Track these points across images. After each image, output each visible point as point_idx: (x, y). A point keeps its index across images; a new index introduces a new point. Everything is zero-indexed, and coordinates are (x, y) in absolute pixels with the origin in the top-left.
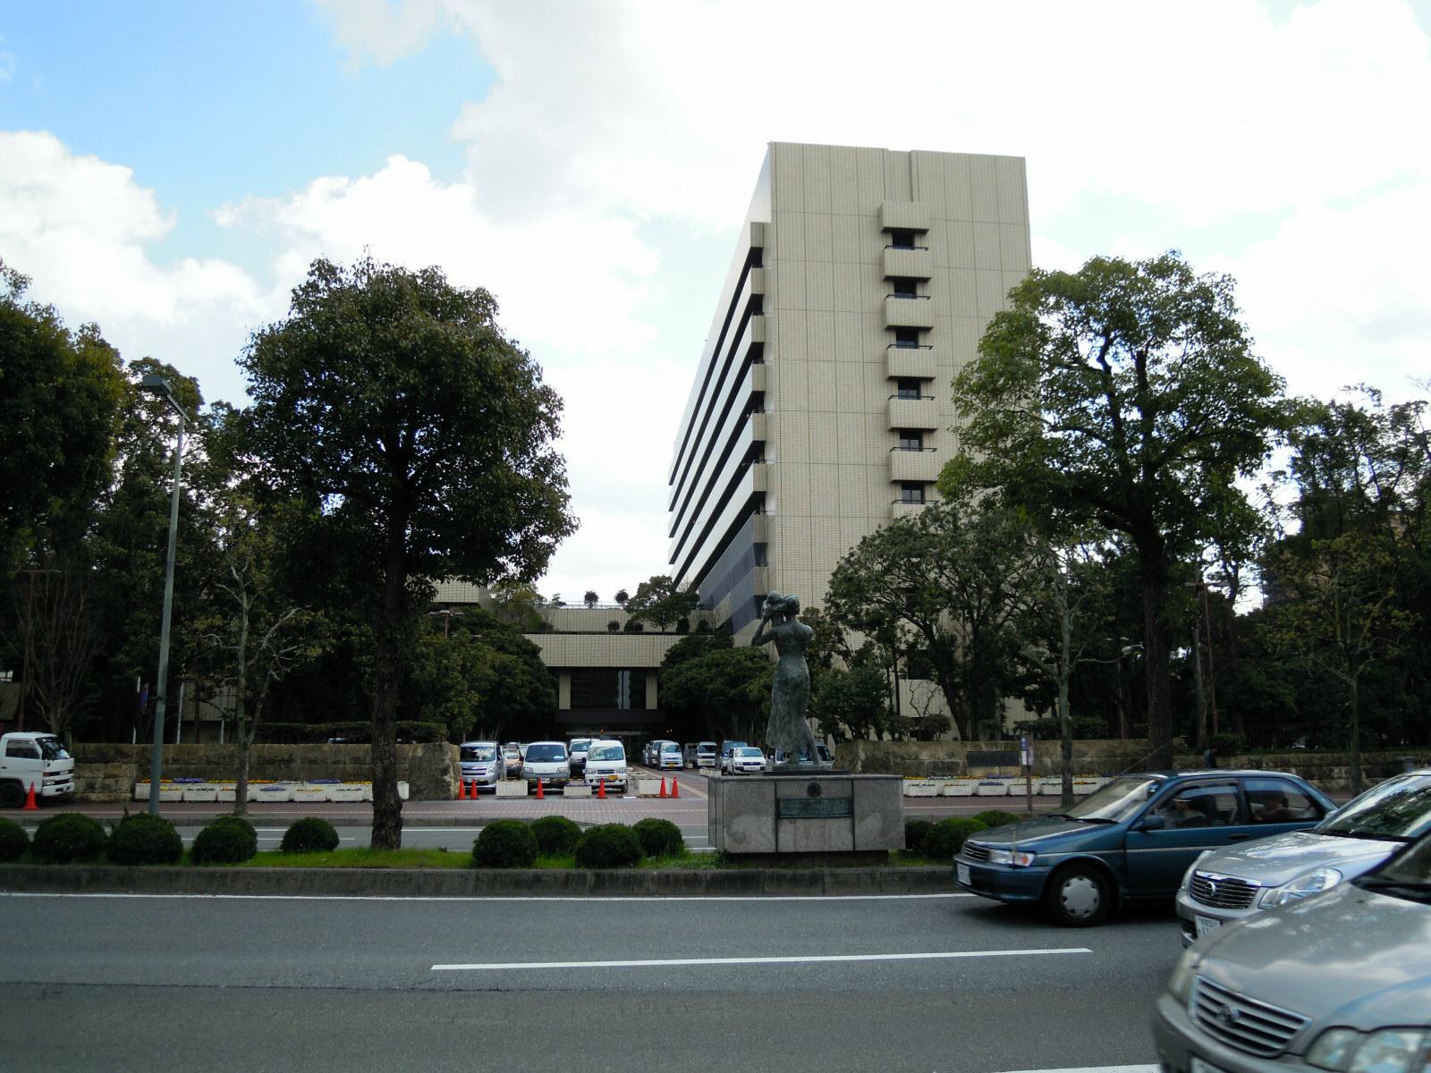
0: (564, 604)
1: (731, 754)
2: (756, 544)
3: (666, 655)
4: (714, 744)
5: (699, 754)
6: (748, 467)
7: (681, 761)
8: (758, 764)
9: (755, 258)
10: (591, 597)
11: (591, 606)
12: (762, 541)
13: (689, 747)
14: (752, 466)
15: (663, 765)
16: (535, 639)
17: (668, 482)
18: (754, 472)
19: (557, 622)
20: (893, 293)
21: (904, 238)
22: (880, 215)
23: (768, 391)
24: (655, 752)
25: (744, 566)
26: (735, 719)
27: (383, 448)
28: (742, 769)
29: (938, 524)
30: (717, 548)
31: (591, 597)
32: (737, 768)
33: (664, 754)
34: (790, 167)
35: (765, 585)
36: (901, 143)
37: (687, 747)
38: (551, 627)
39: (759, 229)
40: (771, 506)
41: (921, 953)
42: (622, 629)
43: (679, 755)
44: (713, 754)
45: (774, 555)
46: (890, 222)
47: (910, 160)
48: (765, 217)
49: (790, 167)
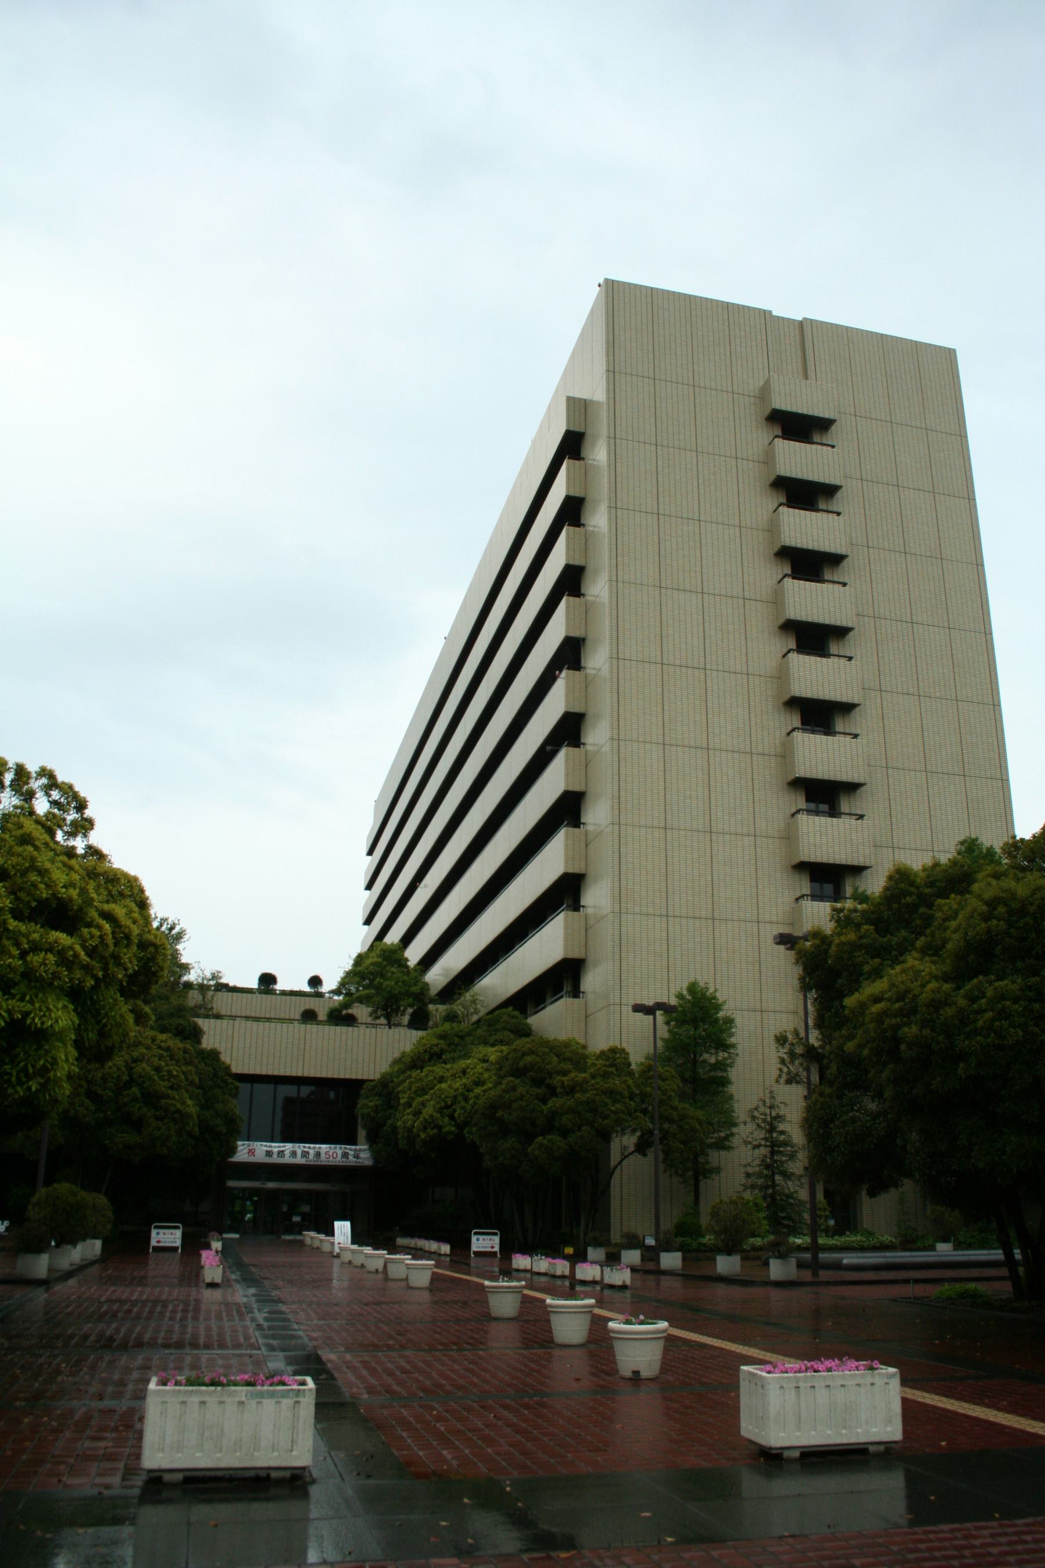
6: (554, 679)
9: (572, 446)
10: (315, 981)
14: (564, 599)
16: (200, 1021)
18: (568, 539)
20: (785, 501)
21: (798, 427)
22: (764, 392)
23: (589, 497)
27: (648, 1514)
29: (673, 1170)
31: (315, 981)
34: (633, 318)
36: (789, 307)
39: (578, 407)
41: (955, 1414)
42: (322, 1016)
47: (804, 330)
48: (595, 390)
49: (633, 318)
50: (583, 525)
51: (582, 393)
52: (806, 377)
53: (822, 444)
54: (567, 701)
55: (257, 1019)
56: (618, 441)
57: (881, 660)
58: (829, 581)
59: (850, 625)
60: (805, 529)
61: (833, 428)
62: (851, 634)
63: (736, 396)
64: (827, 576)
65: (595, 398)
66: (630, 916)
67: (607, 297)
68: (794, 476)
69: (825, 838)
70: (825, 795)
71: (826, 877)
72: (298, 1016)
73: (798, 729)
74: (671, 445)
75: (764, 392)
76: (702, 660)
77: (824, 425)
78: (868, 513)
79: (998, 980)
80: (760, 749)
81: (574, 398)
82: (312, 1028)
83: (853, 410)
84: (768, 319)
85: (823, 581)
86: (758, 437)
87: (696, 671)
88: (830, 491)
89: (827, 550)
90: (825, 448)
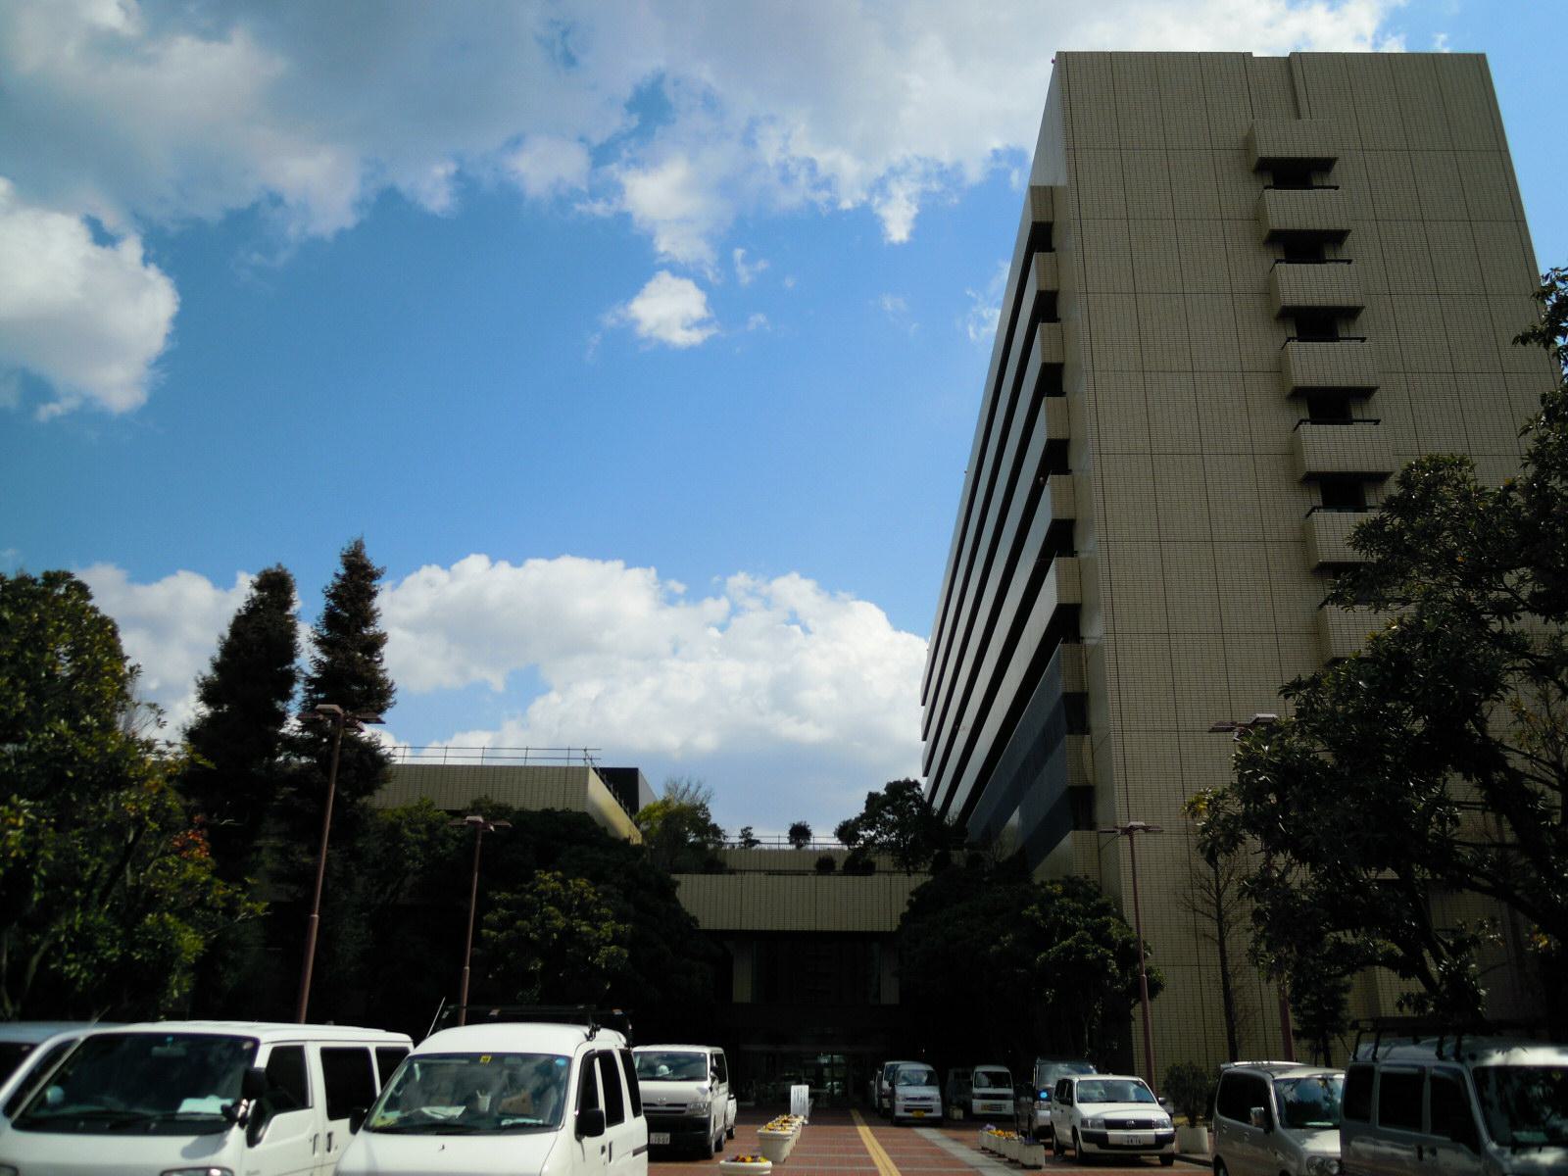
0: (758, 842)
1: (1064, 1093)
2: (1066, 696)
3: (910, 903)
4: (1005, 1070)
5: (976, 1091)
7: (937, 1104)
8: (1147, 1124)
9: (1040, 238)
10: (800, 833)
11: (799, 846)
12: (1077, 689)
13: (957, 1075)
14: (1045, 399)
15: (900, 1113)
17: (920, 702)
19: (731, 863)
21: (1295, 173)
22: (1248, 143)
24: (885, 1085)
25: (1046, 744)
26: (1500, 692)
28: (1101, 1140)
30: (1014, 624)
32: (1089, 1137)
33: (903, 1090)
35: (1088, 767)
37: (951, 1077)
38: (724, 864)
39: (1042, 196)
40: (1095, 630)
42: (839, 866)
43: (933, 1092)
44: (1010, 1091)
45: (1105, 715)
46: (1269, 149)
50: (1060, 320)
51: (1045, 181)
52: (1299, 117)
53: (1337, 261)
54: (1053, 510)
55: (780, 873)
56: (1084, 222)
57: (1418, 420)
58: (1331, 261)
59: (1373, 384)
60: (1308, 284)
61: (1336, 166)
62: (1377, 394)
63: (1216, 153)
64: (1356, 414)
65: (1059, 184)
66: (1135, 734)
67: (1061, 71)
68: (1290, 227)
69: (1333, 447)
70: (1331, 405)
71: (1340, 490)
72: (813, 868)
73: (1319, 508)
74: (1144, 217)
75: (1248, 143)
76: (1198, 445)
77: (1325, 165)
78: (1386, 256)
79: (1537, 605)
80: (1275, 536)
81: (1039, 188)
82: (825, 880)
83: (1359, 143)
84: (1248, 62)
85: (1338, 339)
86: (1242, 192)
87: (1192, 458)
88: (1338, 237)
89: (1337, 303)
90: (1340, 264)
